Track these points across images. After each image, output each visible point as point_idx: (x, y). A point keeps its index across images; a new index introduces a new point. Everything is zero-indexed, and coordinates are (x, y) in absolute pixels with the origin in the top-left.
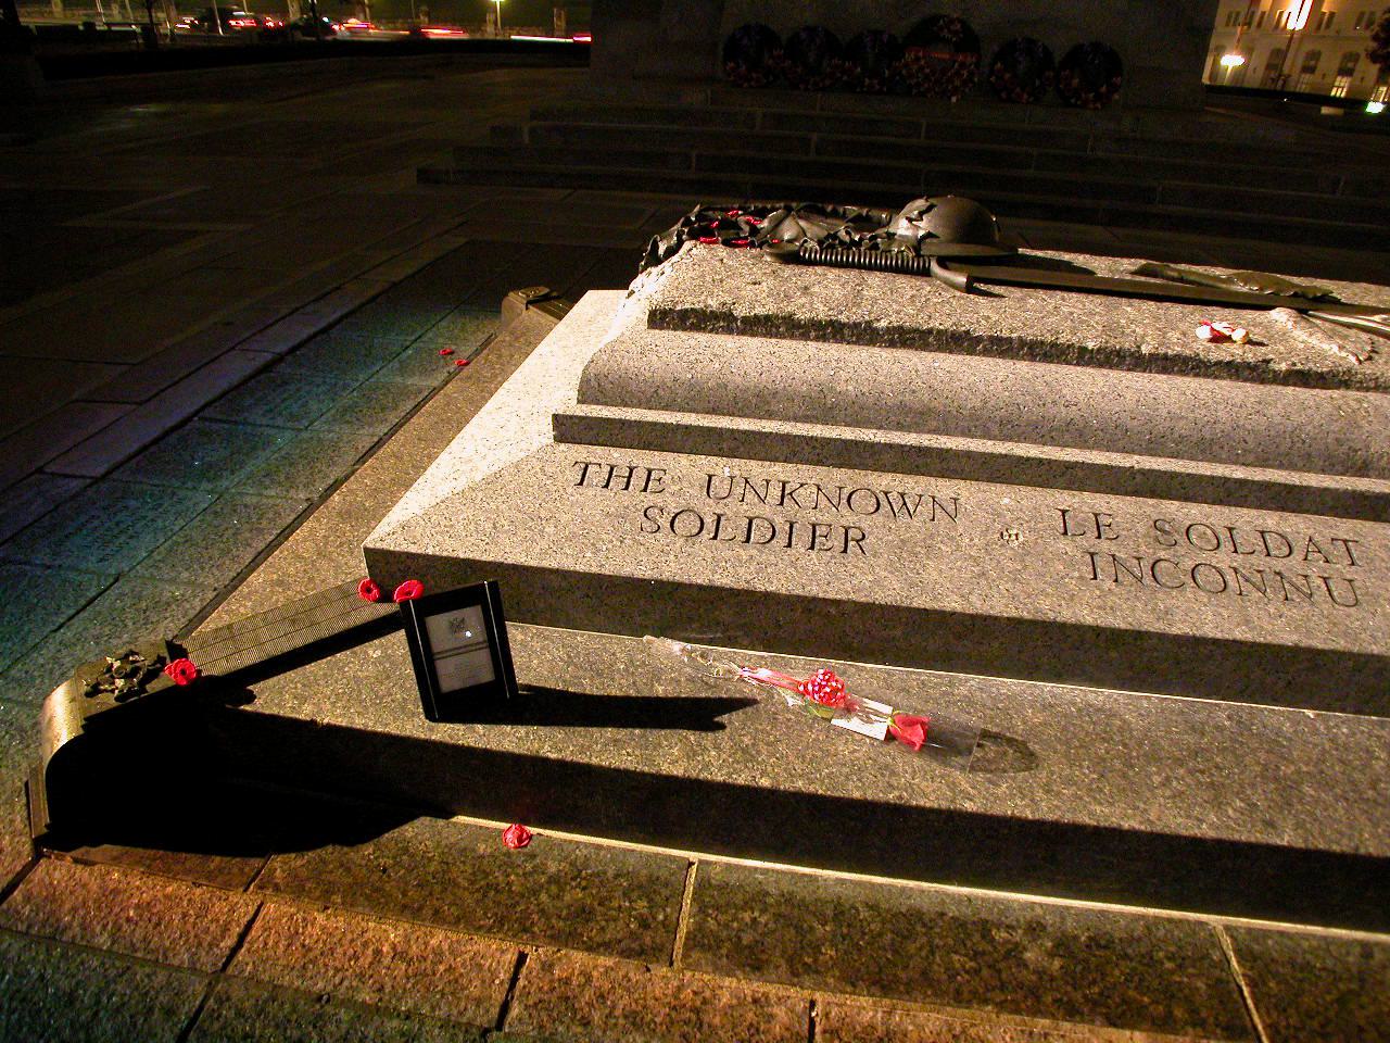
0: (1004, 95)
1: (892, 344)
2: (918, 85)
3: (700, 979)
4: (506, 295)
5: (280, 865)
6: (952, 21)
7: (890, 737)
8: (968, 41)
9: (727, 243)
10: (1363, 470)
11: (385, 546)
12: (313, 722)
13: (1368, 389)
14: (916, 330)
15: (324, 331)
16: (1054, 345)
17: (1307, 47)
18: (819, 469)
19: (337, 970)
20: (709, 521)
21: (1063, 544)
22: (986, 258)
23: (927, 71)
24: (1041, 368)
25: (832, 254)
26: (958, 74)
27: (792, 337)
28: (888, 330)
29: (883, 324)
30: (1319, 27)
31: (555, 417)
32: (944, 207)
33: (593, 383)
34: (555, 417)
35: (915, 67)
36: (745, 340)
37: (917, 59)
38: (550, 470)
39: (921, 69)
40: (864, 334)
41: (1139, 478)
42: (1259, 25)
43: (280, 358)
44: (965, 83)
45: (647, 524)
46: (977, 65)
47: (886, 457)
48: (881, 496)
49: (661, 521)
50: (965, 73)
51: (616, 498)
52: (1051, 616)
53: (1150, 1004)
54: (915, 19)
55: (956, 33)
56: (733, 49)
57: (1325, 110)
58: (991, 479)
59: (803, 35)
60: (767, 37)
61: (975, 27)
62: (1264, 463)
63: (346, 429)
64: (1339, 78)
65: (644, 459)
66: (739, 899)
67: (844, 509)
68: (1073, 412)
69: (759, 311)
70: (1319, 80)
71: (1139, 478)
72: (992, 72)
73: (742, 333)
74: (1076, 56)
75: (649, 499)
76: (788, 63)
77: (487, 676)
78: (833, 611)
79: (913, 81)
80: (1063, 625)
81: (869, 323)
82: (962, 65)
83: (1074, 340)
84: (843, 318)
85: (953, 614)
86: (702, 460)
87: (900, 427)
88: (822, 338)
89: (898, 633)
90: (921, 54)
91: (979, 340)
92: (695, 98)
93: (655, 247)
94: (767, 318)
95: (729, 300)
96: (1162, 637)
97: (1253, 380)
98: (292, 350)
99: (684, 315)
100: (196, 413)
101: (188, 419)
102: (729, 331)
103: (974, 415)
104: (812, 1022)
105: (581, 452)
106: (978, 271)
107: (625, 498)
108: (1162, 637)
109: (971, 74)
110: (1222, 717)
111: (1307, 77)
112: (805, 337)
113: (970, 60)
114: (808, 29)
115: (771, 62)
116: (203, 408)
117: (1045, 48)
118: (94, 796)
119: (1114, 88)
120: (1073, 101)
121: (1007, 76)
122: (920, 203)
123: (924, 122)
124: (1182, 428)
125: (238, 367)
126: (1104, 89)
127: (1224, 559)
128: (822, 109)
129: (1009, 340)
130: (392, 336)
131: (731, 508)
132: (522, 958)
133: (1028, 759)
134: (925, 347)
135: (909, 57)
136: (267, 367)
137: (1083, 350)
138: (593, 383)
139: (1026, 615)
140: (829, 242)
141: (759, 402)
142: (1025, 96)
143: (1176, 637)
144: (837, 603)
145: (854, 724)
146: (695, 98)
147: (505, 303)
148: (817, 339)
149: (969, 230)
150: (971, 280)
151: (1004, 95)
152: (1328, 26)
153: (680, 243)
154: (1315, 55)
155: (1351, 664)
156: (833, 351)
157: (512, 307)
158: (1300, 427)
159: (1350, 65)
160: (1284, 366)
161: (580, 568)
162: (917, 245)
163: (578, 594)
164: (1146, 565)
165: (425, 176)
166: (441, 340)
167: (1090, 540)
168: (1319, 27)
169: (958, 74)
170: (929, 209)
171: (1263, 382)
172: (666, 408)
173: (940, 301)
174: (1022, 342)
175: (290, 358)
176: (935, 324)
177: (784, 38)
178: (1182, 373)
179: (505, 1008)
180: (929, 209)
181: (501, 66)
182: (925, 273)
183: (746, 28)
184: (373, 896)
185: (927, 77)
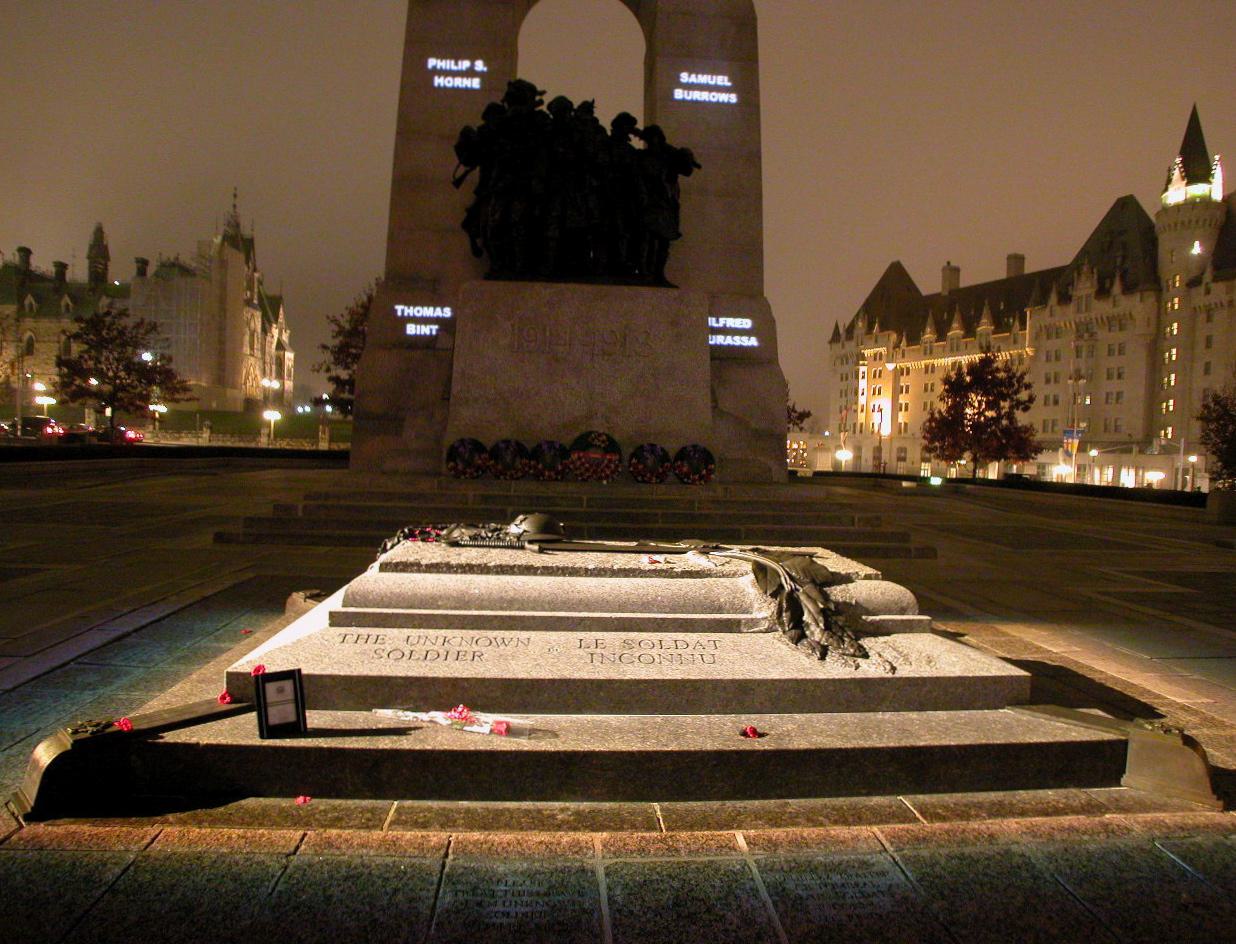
0: (640, 478)
1: (497, 573)
2: (581, 474)
3: (397, 833)
4: (290, 595)
5: (171, 817)
6: (600, 435)
7: (491, 731)
8: (612, 446)
9: (423, 540)
10: (720, 610)
11: (238, 670)
12: (198, 744)
13: (720, 577)
14: (508, 566)
15: (158, 620)
16: (572, 568)
17: (897, 444)
18: (464, 631)
19: (208, 844)
20: (407, 653)
21: (581, 652)
22: (551, 536)
23: (587, 465)
24: (567, 579)
25: (476, 541)
26: (607, 466)
27: (450, 573)
28: (495, 567)
29: (493, 564)
30: (900, 432)
31: (331, 613)
32: (531, 518)
33: (351, 597)
34: (331, 613)
35: (578, 463)
36: (427, 575)
37: (579, 458)
38: (326, 638)
39: (583, 464)
40: (484, 569)
41: (616, 622)
42: (861, 432)
43: (128, 634)
44: (613, 472)
45: (376, 656)
46: (620, 461)
47: (495, 622)
48: (493, 640)
49: (383, 654)
50: (613, 466)
51: (361, 646)
52: (568, 677)
53: (326, 402)
54: (577, 434)
55: (603, 442)
56: (453, 453)
57: (905, 484)
58: (546, 629)
59: (502, 445)
60: (477, 447)
61: (616, 437)
62: (674, 611)
63: (183, 667)
64: (923, 464)
65: (374, 631)
66: (418, 811)
67: (474, 645)
68: (582, 596)
69: (434, 561)
70: (910, 465)
71: (616, 622)
72: (630, 465)
73: (425, 572)
74: (683, 454)
75: (377, 646)
76: (492, 462)
77: (292, 718)
78: (466, 685)
79: (578, 472)
80: (574, 680)
81: (486, 564)
82: (610, 461)
83: (583, 566)
84: (474, 563)
85: (522, 680)
86: (405, 630)
87: (502, 609)
88: (464, 572)
89: (498, 694)
90: (581, 455)
91: (538, 568)
92: (425, 485)
93: (385, 545)
94: (437, 564)
95: (419, 558)
96: (621, 681)
97: (667, 577)
98: (136, 631)
99: (397, 564)
100: (72, 660)
101: (68, 663)
102: (419, 571)
103: (535, 601)
104: (450, 842)
105: (343, 630)
106: (544, 545)
107: (366, 647)
108: (621, 681)
109: (617, 466)
110: (659, 720)
111: (901, 464)
112: (456, 572)
113: (615, 457)
114: (504, 441)
115: (480, 462)
116: (79, 656)
117: (662, 449)
118: (67, 791)
119: (710, 472)
120: (686, 480)
121: (641, 467)
122: (521, 517)
123: (585, 498)
124: (633, 598)
125: (97, 639)
126: (704, 472)
127: (655, 652)
128: (515, 491)
129: (552, 567)
130: (208, 624)
131: (417, 648)
132: (305, 835)
133: (556, 736)
134: (513, 573)
135: (575, 456)
136: (119, 639)
137: (587, 570)
138: (351, 597)
139: (556, 677)
140: (473, 538)
141: (431, 601)
142: (654, 479)
143: (628, 681)
144: (467, 680)
145: (475, 728)
146: (425, 485)
147: (289, 600)
148: (462, 573)
149: (545, 528)
150: (540, 548)
151: (640, 478)
152: (906, 430)
153: (399, 542)
154: (903, 450)
155: (710, 686)
156: (469, 577)
157: (294, 603)
158: (686, 593)
159: (903, 455)
160: (680, 570)
161: (342, 673)
162: (519, 537)
163: (340, 688)
164: (617, 657)
165: (219, 538)
166: (242, 626)
167: (592, 649)
168: (900, 432)
169: (607, 466)
170: (525, 519)
171: (672, 577)
172: (387, 607)
173: (530, 556)
174: (558, 568)
175: (134, 634)
176: (518, 563)
177: (488, 449)
178: (635, 576)
179: (297, 848)
180: (525, 519)
181: (273, 467)
182: (522, 548)
183: (462, 441)
184: (228, 821)
185: (587, 470)
